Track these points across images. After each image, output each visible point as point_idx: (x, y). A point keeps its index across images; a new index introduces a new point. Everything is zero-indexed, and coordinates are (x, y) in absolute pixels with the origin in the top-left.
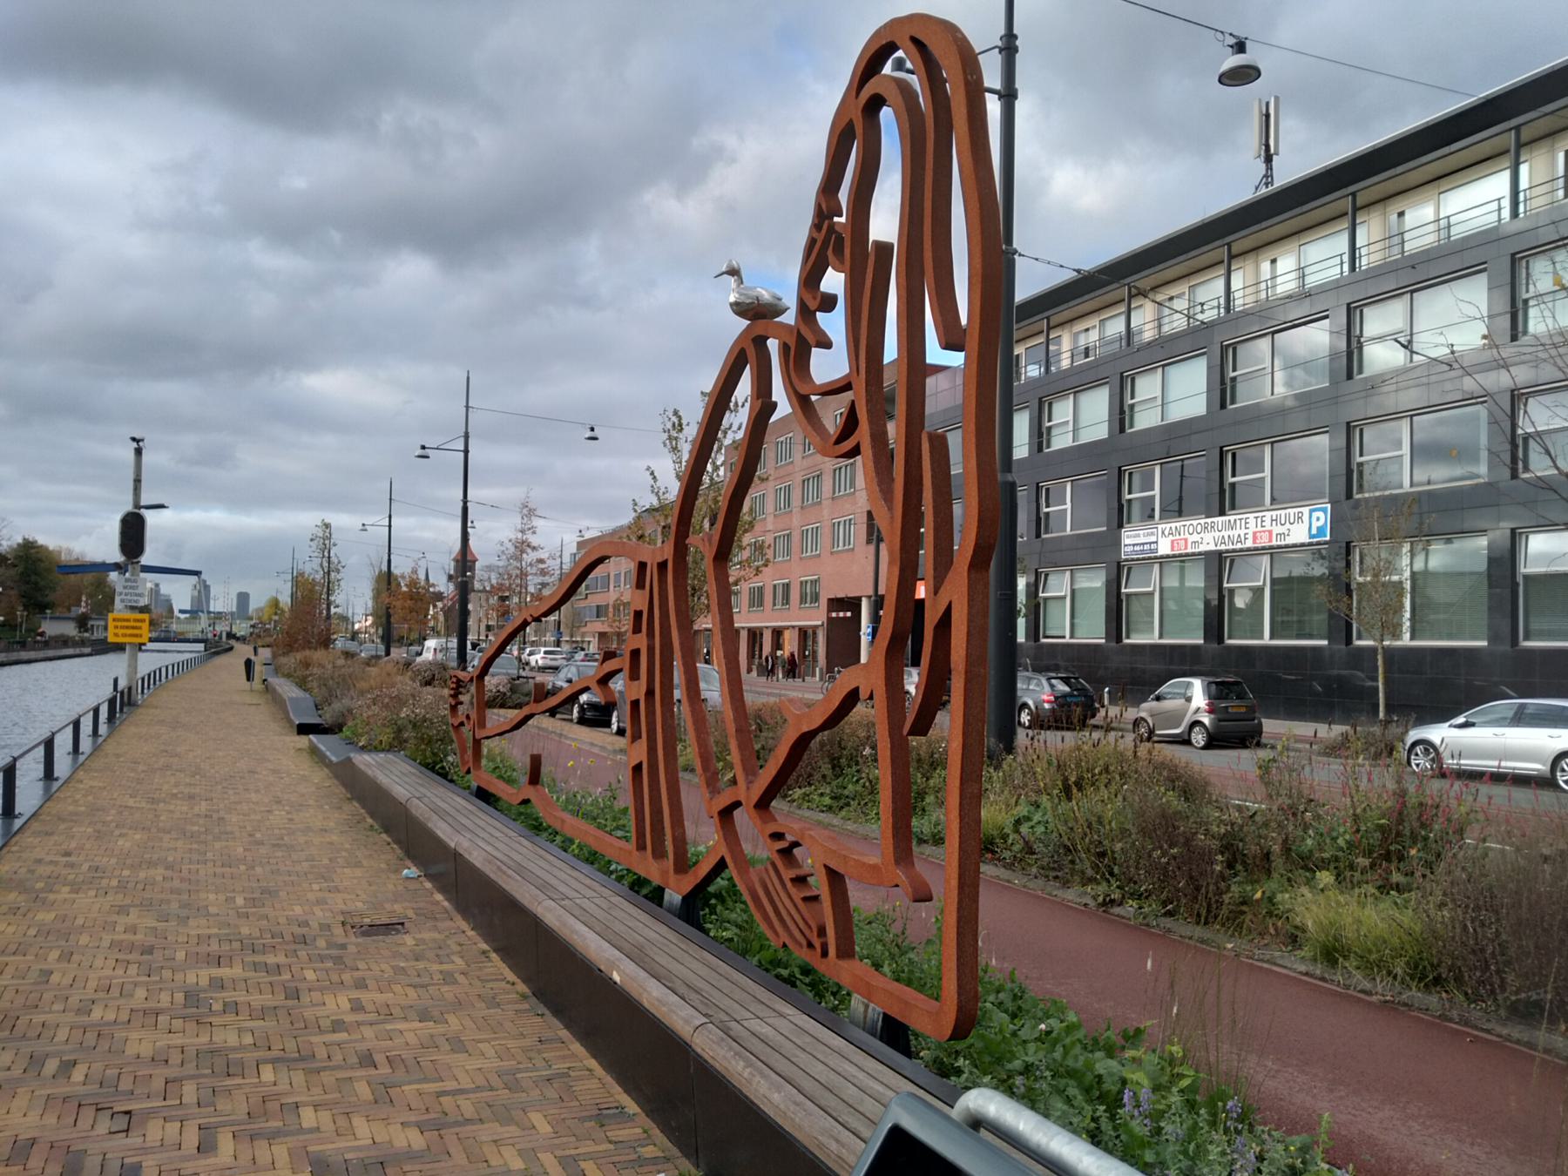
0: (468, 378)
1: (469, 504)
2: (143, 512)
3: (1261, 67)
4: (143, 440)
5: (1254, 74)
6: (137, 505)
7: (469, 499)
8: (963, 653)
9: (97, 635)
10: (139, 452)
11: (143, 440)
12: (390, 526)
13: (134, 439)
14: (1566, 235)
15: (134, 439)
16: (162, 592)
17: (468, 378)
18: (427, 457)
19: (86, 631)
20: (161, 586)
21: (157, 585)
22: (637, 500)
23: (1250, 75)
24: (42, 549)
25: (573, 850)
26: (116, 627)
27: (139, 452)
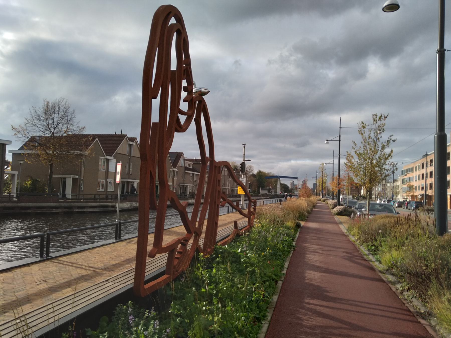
0: (340, 119)
1: (340, 156)
2: (245, 162)
3: (400, 4)
4: (245, 144)
5: (385, 9)
6: (244, 161)
7: (340, 154)
8: (156, 174)
9: (273, 194)
10: (244, 147)
11: (245, 144)
12: (333, 164)
13: (243, 144)
14: (450, 50)
15: (243, 144)
16: (295, 183)
17: (340, 119)
18: (328, 143)
19: (270, 193)
20: (295, 182)
21: (293, 181)
22: (348, 151)
23: (386, 9)
24: (264, 173)
25: (8, 193)
26: (240, 190)
27: (244, 147)
